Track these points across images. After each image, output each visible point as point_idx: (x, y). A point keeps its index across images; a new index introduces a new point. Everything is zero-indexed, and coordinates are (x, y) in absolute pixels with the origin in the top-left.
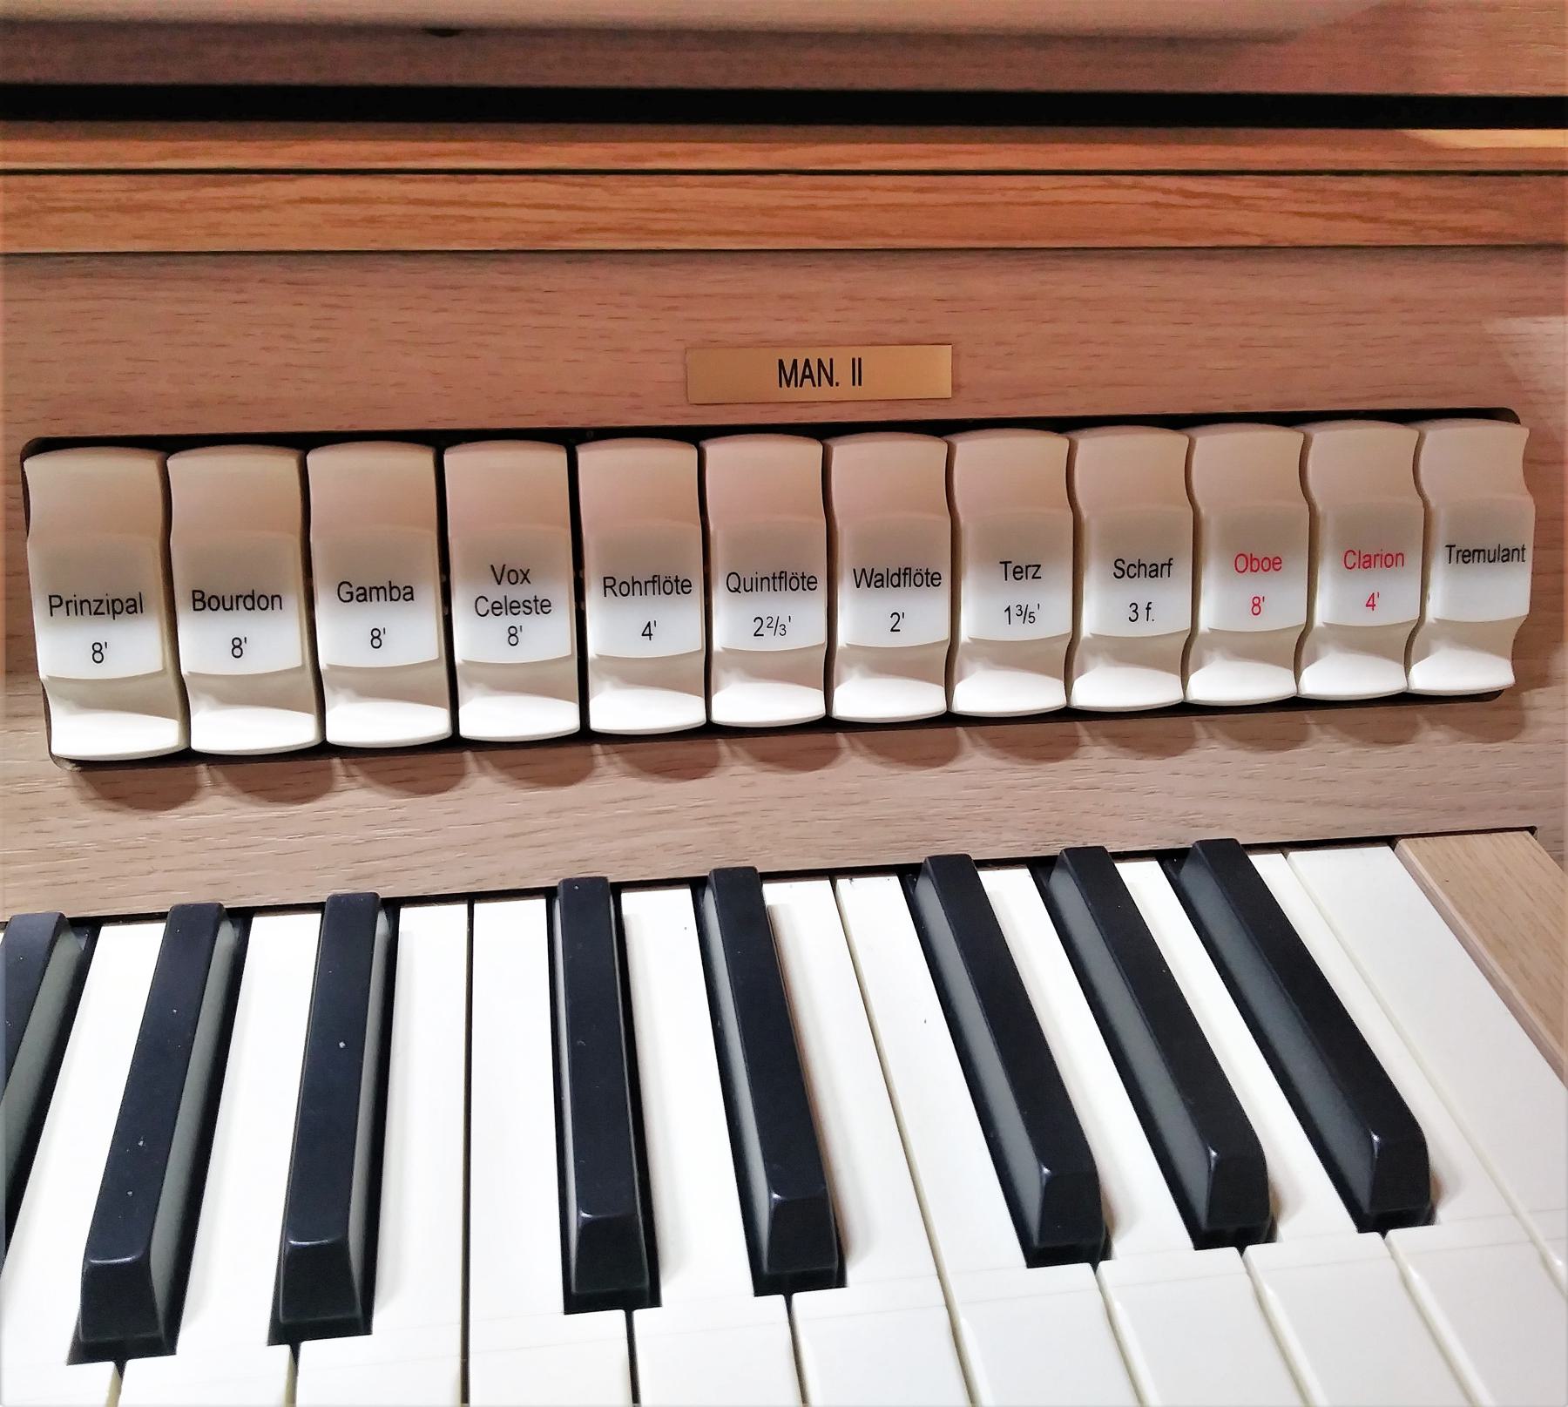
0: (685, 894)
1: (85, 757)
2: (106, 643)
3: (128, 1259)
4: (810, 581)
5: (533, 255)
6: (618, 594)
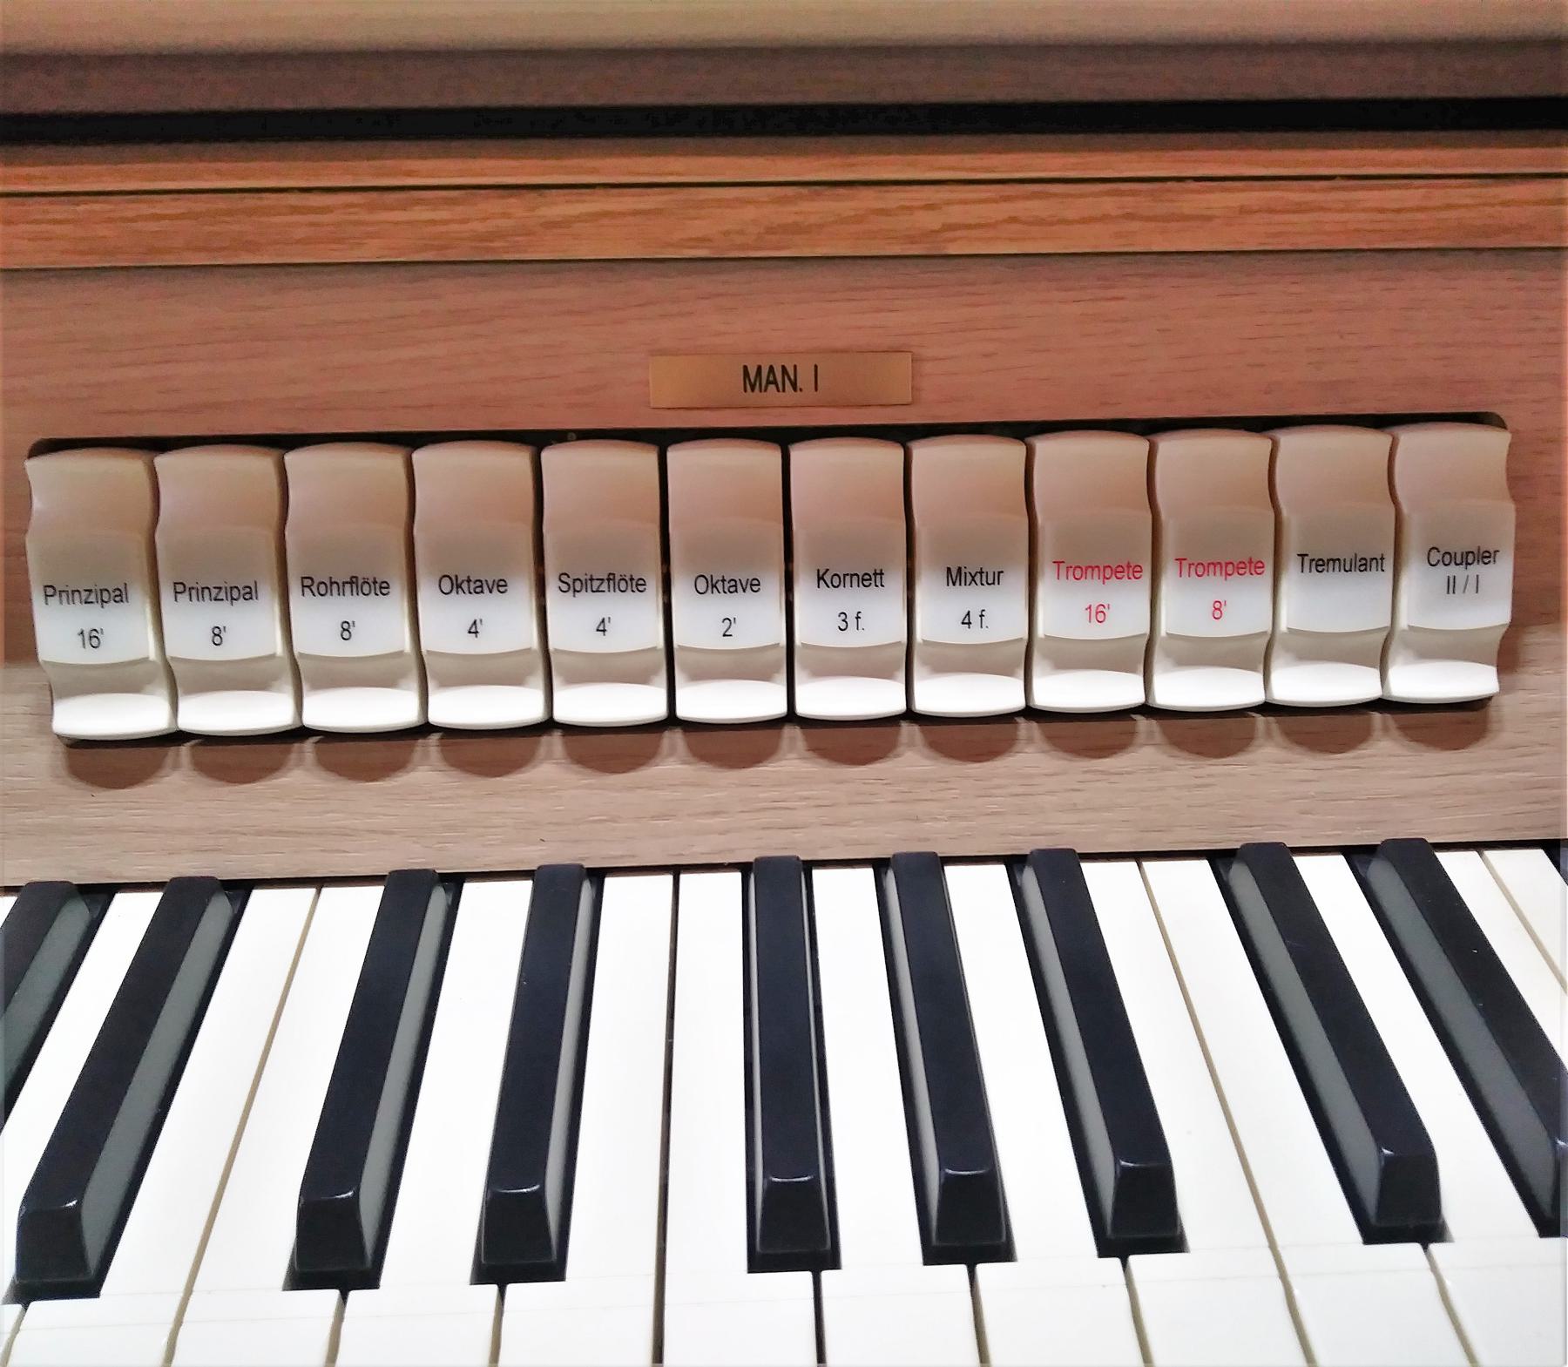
0: (868, 873)
1: (456, 725)
2: (224, 627)
3: (806, 1179)
4: (1135, 570)
5: (988, 261)
6: (316, 593)
